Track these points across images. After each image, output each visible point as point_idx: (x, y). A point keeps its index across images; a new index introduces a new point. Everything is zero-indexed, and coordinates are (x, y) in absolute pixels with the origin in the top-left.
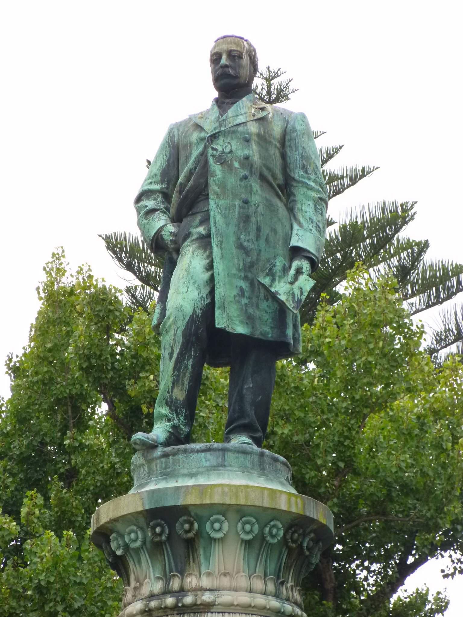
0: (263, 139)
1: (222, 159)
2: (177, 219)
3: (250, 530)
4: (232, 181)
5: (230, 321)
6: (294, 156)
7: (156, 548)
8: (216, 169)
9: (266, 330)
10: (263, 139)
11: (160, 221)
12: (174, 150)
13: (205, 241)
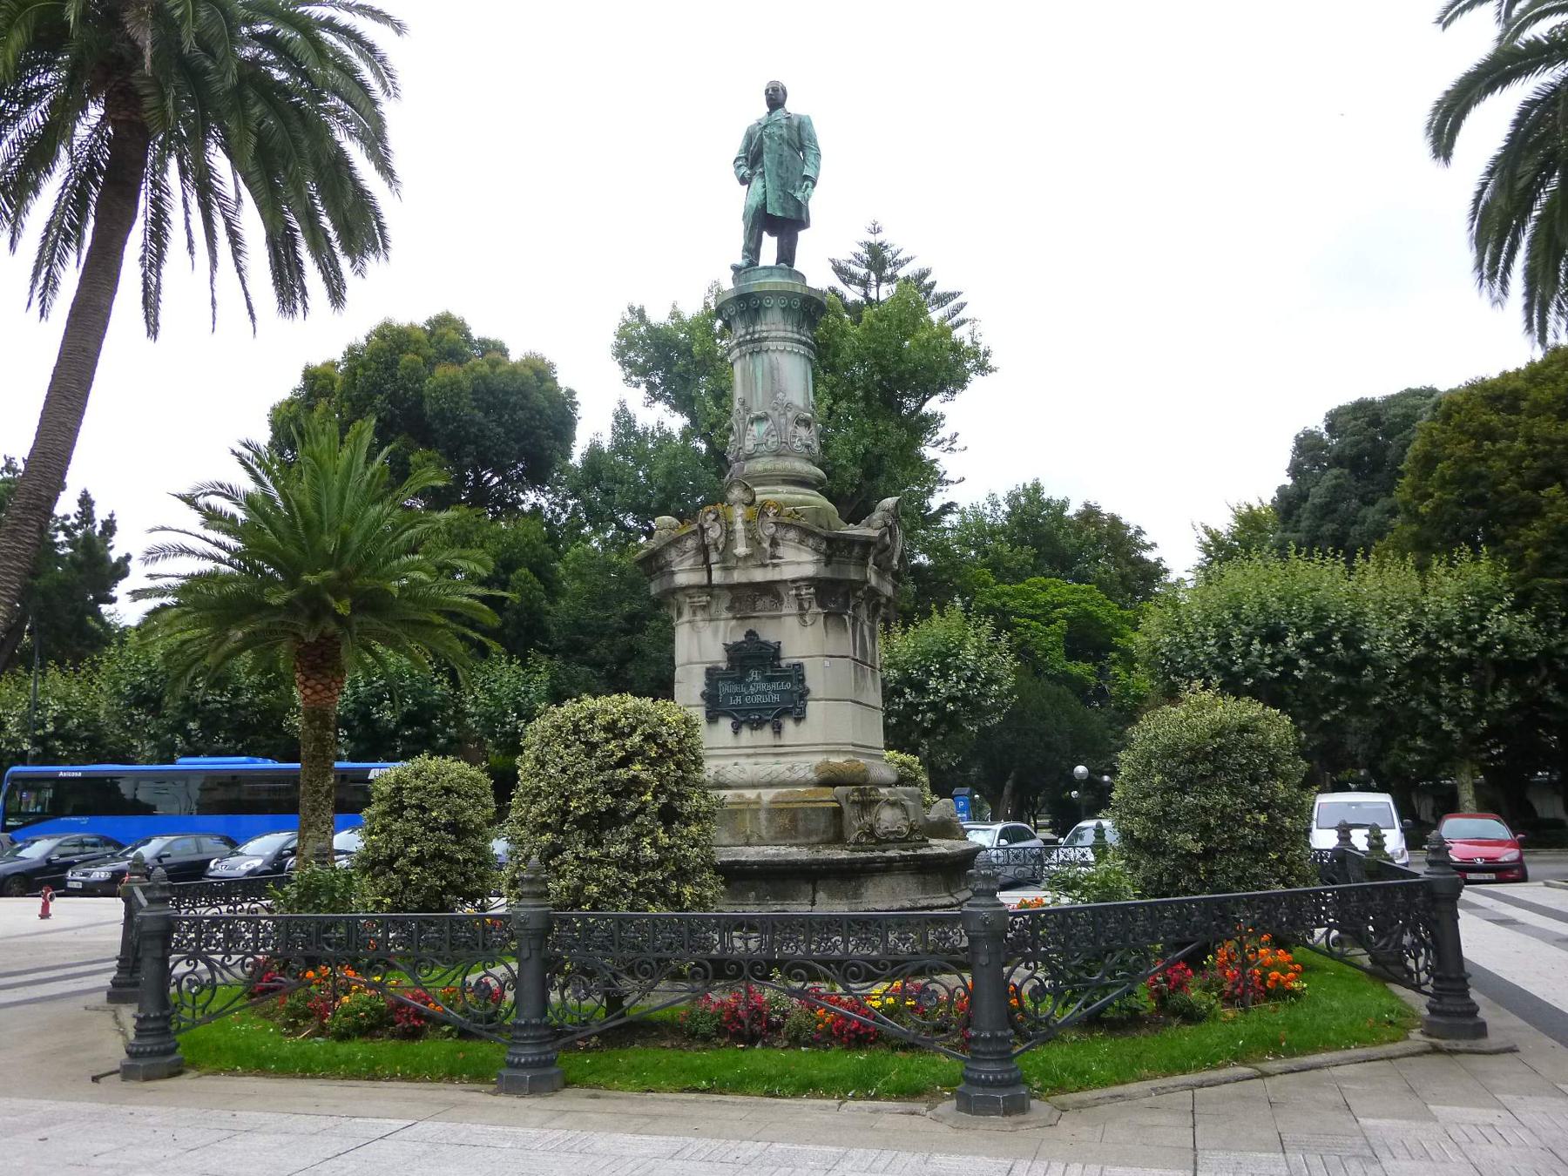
0: (789, 127)
1: (770, 136)
2: (751, 168)
3: (783, 302)
4: (774, 146)
5: (774, 210)
6: (804, 135)
7: (742, 314)
8: (766, 140)
9: (792, 214)
10: (789, 127)
11: (744, 170)
12: (749, 137)
13: (762, 174)
